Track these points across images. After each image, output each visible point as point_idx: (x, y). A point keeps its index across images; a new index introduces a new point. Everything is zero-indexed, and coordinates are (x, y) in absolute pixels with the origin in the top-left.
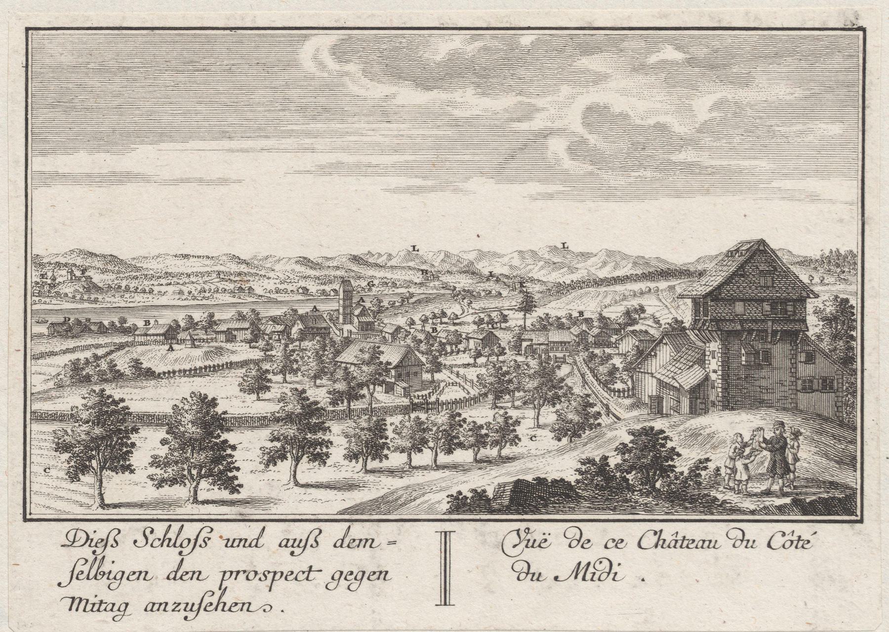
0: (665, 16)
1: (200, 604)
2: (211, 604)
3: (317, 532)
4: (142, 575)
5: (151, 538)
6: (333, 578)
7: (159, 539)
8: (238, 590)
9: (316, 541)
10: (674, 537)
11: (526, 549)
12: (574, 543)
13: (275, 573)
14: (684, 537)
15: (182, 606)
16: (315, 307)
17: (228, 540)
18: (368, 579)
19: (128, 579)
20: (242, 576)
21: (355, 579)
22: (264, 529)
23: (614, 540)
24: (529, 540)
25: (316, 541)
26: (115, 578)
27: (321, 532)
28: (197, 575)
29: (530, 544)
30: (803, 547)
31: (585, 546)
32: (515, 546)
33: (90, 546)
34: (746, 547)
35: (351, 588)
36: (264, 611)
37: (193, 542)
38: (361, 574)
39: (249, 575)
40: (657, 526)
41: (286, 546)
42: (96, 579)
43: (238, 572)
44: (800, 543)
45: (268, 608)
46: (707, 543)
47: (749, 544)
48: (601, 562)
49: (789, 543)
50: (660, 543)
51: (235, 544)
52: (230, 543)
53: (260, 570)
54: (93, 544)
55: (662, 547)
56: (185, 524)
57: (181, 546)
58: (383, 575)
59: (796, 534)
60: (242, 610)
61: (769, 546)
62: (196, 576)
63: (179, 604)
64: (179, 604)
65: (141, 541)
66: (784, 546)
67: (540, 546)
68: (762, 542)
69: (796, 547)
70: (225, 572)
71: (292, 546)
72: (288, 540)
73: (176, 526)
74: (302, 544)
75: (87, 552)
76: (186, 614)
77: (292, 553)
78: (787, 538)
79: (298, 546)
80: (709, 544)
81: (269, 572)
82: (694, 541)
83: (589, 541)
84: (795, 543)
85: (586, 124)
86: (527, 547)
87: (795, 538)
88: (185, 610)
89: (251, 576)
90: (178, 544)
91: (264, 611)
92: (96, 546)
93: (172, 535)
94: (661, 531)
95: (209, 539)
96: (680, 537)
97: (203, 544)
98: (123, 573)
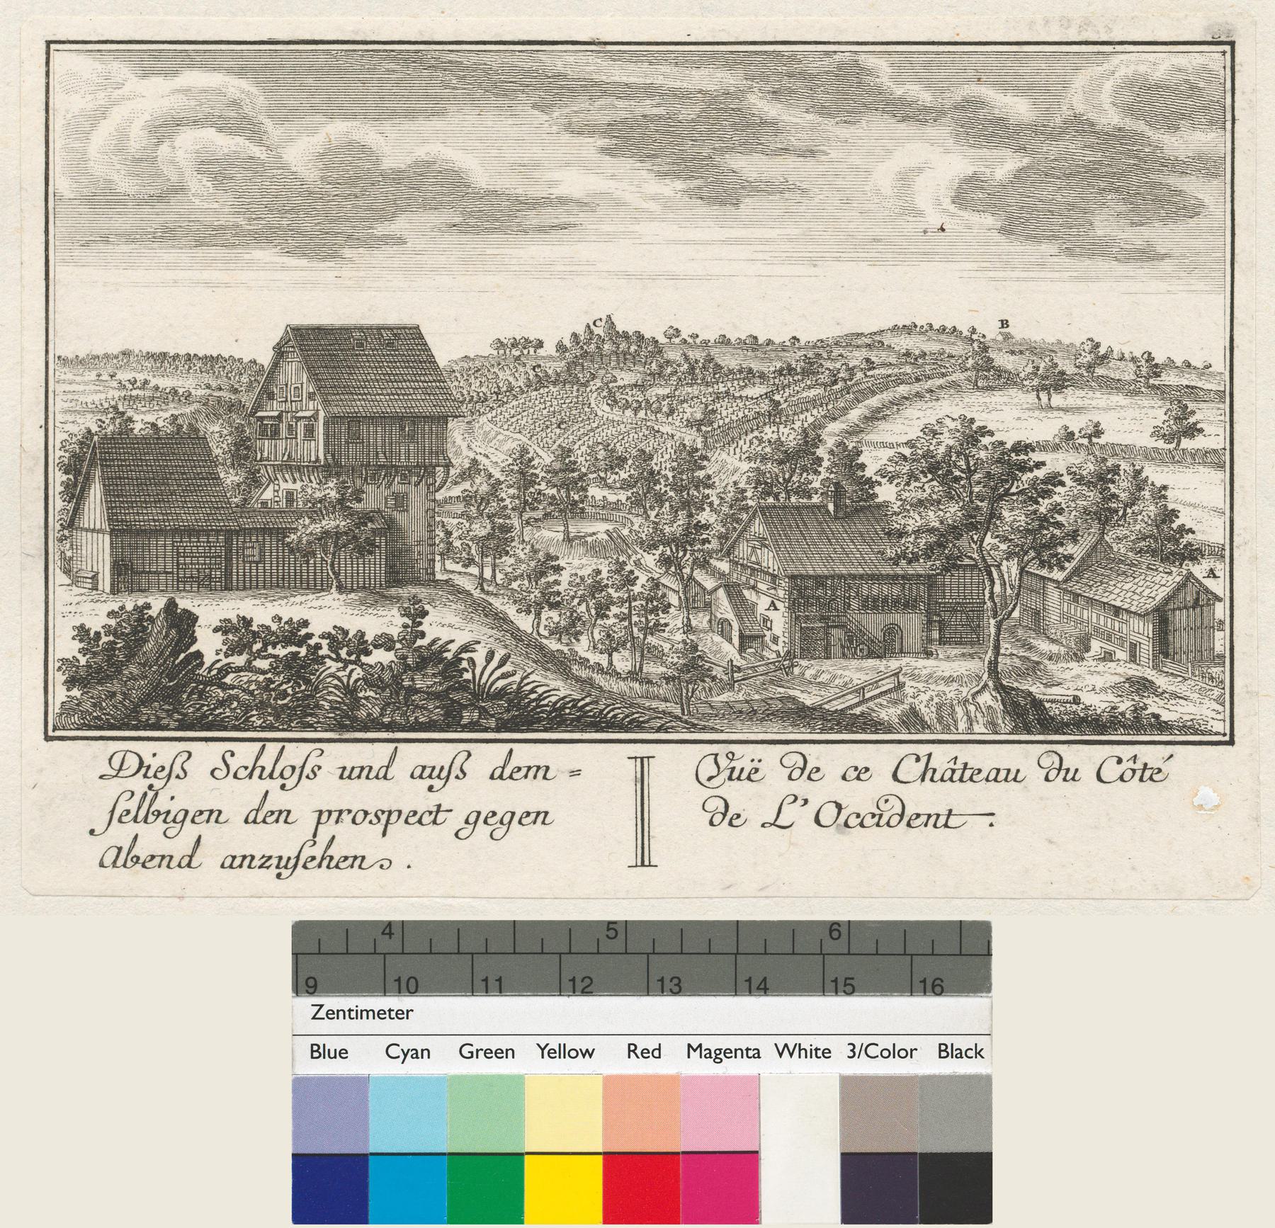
0: (1066, 22)
1: (298, 857)
2: (313, 858)
3: (185, 755)
4: (214, 815)
5: (234, 763)
6: (467, 822)
7: (246, 768)
8: (349, 839)
9: (462, 770)
10: (951, 765)
11: (728, 783)
13: (390, 813)
14: (1146, 765)
15: (274, 861)
17: (344, 768)
18: (520, 822)
20: (347, 818)
21: (501, 823)
22: (511, 751)
23: (856, 769)
24: (733, 769)
25: (462, 770)
26: (174, 821)
27: (469, 755)
28: (283, 816)
29: (735, 775)
32: (710, 779)
33: (145, 776)
34: (1065, 780)
36: (381, 866)
37: (298, 771)
38: (509, 815)
39: (360, 817)
40: (923, 750)
41: (421, 777)
42: (146, 822)
44: (1148, 774)
45: (386, 864)
47: (1071, 776)
48: (887, 801)
49: (1129, 773)
51: (357, 772)
52: (345, 774)
53: (372, 810)
54: (150, 773)
55: (932, 780)
56: (268, 744)
57: (282, 775)
58: (541, 817)
60: (352, 866)
63: (270, 858)
64: (270, 858)
66: (1121, 778)
67: (749, 778)
68: (1087, 774)
69: (1141, 780)
70: (321, 812)
71: (430, 776)
72: (998, 770)
74: (444, 774)
75: (139, 784)
76: (429, 782)
78: (1125, 765)
79: (439, 777)
80: (1014, 777)
81: (383, 812)
83: (818, 770)
84: (1138, 774)
85: (1129, 110)
86: (730, 778)
87: (1139, 766)
88: (278, 867)
89: (360, 816)
90: (276, 774)
91: (381, 866)
92: (155, 776)
93: (267, 761)
94: (930, 755)
95: (320, 768)
97: (311, 776)
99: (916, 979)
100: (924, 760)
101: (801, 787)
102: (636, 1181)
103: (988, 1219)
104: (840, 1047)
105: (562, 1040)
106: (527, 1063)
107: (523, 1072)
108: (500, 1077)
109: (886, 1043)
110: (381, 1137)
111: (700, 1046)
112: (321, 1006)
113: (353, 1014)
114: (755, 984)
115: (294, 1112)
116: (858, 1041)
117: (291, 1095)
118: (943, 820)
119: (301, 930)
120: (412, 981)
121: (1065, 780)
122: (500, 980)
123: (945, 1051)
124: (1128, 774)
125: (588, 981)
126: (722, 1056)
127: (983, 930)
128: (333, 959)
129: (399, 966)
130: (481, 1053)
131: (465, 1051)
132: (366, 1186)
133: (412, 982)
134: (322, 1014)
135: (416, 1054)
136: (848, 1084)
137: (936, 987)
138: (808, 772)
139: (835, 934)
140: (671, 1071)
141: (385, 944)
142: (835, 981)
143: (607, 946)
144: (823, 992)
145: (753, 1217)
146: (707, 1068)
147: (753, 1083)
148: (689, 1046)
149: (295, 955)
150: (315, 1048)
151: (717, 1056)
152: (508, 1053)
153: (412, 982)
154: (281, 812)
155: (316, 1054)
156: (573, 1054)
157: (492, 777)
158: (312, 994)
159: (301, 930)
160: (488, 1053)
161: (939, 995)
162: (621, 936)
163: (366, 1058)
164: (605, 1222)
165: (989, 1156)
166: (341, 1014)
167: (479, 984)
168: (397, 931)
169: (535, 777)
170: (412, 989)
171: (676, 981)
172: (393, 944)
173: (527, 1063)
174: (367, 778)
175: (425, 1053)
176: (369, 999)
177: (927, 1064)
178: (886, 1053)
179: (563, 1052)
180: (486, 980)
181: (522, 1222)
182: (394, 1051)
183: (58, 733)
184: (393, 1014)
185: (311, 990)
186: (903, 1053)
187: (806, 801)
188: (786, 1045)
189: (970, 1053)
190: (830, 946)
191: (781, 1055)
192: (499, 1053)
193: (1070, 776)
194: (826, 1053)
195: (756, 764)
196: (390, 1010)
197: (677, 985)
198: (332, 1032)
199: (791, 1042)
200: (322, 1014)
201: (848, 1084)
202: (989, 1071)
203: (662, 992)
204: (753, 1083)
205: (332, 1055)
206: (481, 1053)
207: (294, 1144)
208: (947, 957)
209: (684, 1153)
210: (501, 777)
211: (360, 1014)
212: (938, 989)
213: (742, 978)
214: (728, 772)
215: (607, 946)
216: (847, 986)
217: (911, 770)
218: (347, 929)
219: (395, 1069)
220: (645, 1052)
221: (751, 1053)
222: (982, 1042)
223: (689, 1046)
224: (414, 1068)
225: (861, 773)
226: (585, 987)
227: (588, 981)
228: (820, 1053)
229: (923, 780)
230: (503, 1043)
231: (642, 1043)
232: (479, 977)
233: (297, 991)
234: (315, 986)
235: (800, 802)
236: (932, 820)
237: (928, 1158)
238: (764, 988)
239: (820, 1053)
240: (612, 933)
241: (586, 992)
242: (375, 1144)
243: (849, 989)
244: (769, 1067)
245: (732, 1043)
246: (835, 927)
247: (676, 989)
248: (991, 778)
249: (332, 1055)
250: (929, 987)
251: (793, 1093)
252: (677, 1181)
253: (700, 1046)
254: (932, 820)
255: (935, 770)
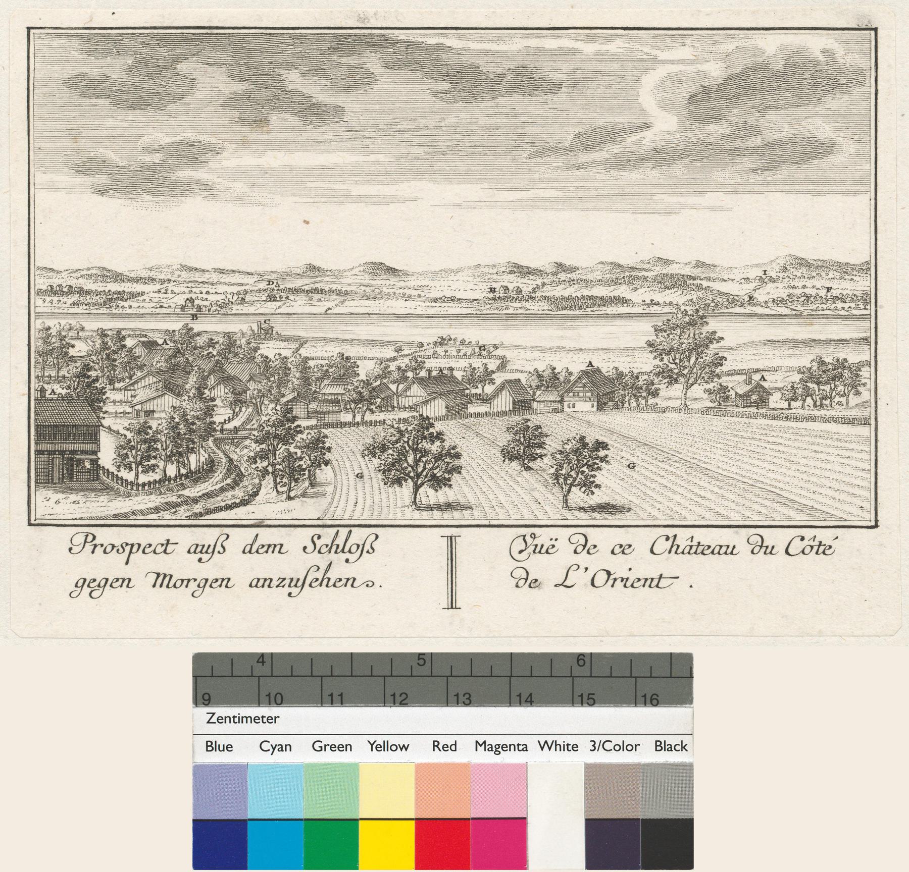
3: (374, 537)
5: (319, 543)
6: (76, 586)
10: (689, 543)
12: (580, 549)
16: (763, 377)
19: (111, 586)
21: (99, 586)
23: (621, 546)
24: (536, 546)
27: (377, 537)
30: (824, 553)
31: (591, 551)
32: (521, 552)
35: (93, 595)
41: (195, 552)
43: (189, 580)
44: (822, 549)
46: (724, 549)
47: (769, 551)
49: (809, 548)
50: (674, 549)
56: (354, 530)
59: (817, 540)
61: (787, 552)
62: (225, 583)
65: (310, 547)
73: (344, 532)
74: (210, 550)
76: (199, 555)
77: (200, 560)
78: (806, 542)
80: (731, 551)
82: (709, 547)
84: (815, 548)
86: (534, 552)
90: (346, 550)
93: (340, 541)
94: (675, 536)
96: (695, 543)
98: (107, 580)
99: (639, 694)
100: (671, 540)
101: (583, 559)
102: (439, 839)
103: (691, 867)
104: (584, 743)
105: (386, 738)
106: (360, 754)
107: (357, 761)
108: (342, 764)
109: (618, 740)
110: (257, 807)
111: (485, 742)
112: (214, 714)
113: (236, 720)
114: (524, 698)
115: (194, 789)
116: (597, 739)
117: (191, 777)
118: (654, 582)
119: (199, 659)
120: (279, 696)
121: (765, 553)
122: (341, 695)
123: (659, 746)
124: (807, 550)
125: (404, 696)
126: (500, 749)
127: (687, 659)
128: (222, 680)
129: (270, 686)
130: (328, 747)
131: (317, 746)
132: (245, 842)
133: (279, 696)
134: (214, 719)
135: (282, 748)
136: (591, 770)
137: (653, 700)
138: (587, 547)
139: (581, 663)
140: (464, 760)
141: (259, 670)
142: (581, 696)
143: (417, 671)
144: (573, 704)
145: (523, 864)
146: (489, 758)
147: (524, 767)
148: (477, 742)
149: (195, 677)
150: (209, 744)
151: (497, 749)
152: (347, 747)
153: (279, 696)
154: (223, 580)
155: (210, 748)
156: (394, 748)
157: (189, 552)
158: (206, 705)
159: (199, 659)
160: (333, 747)
161: (656, 706)
162: (428, 664)
163: (246, 751)
164: (417, 868)
165: (691, 821)
166: (228, 719)
167: (326, 698)
168: (268, 660)
169: (273, 552)
170: (279, 701)
171: (467, 696)
172: (266, 670)
173: (360, 754)
174: (676, 553)
175: (288, 747)
176: (247, 709)
177: (647, 755)
178: (617, 748)
179: (386, 747)
180: (331, 695)
181: (357, 868)
182: (266, 746)
183: (38, 522)
184: (265, 720)
185: (206, 702)
186: (630, 748)
187: (586, 569)
188: (546, 742)
189: (678, 748)
190: (577, 671)
191: (542, 749)
192: (341, 748)
193: (768, 551)
194: (575, 747)
195: (553, 542)
196: (263, 717)
197: (468, 699)
198: (222, 733)
199: (550, 739)
200: (214, 719)
201: (591, 770)
202: (691, 761)
203: (457, 704)
204: (522, 770)
205: (221, 749)
206: (328, 747)
207: (194, 813)
208: (661, 679)
209: (473, 819)
210: (250, 552)
211: (241, 719)
212: (655, 702)
213: (514, 694)
214: (533, 548)
215: (417, 671)
216: (590, 700)
217: (663, 546)
218: (232, 659)
219: (267, 759)
220: (445, 748)
221: (521, 748)
222: (686, 740)
223: (477, 742)
224: (280, 758)
225: (624, 549)
226: (402, 700)
227: (404, 696)
228: (570, 748)
229: (670, 552)
230: (343, 740)
231: (443, 740)
232: (326, 693)
233: (196, 703)
234: (209, 700)
235: (582, 569)
236: (648, 582)
237: (647, 822)
238: (530, 701)
239: (570, 748)
240: (421, 662)
241: (403, 704)
242: (254, 811)
243: (591, 701)
244: (534, 757)
245: (508, 740)
246: (581, 657)
247: (467, 702)
248: (686, 552)
249: (221, 749)
250: (648, 700)
251: (551, 776)
252: (468, 839)
253: (485, 742)
254: (648, 582)
255: (678, 546)
